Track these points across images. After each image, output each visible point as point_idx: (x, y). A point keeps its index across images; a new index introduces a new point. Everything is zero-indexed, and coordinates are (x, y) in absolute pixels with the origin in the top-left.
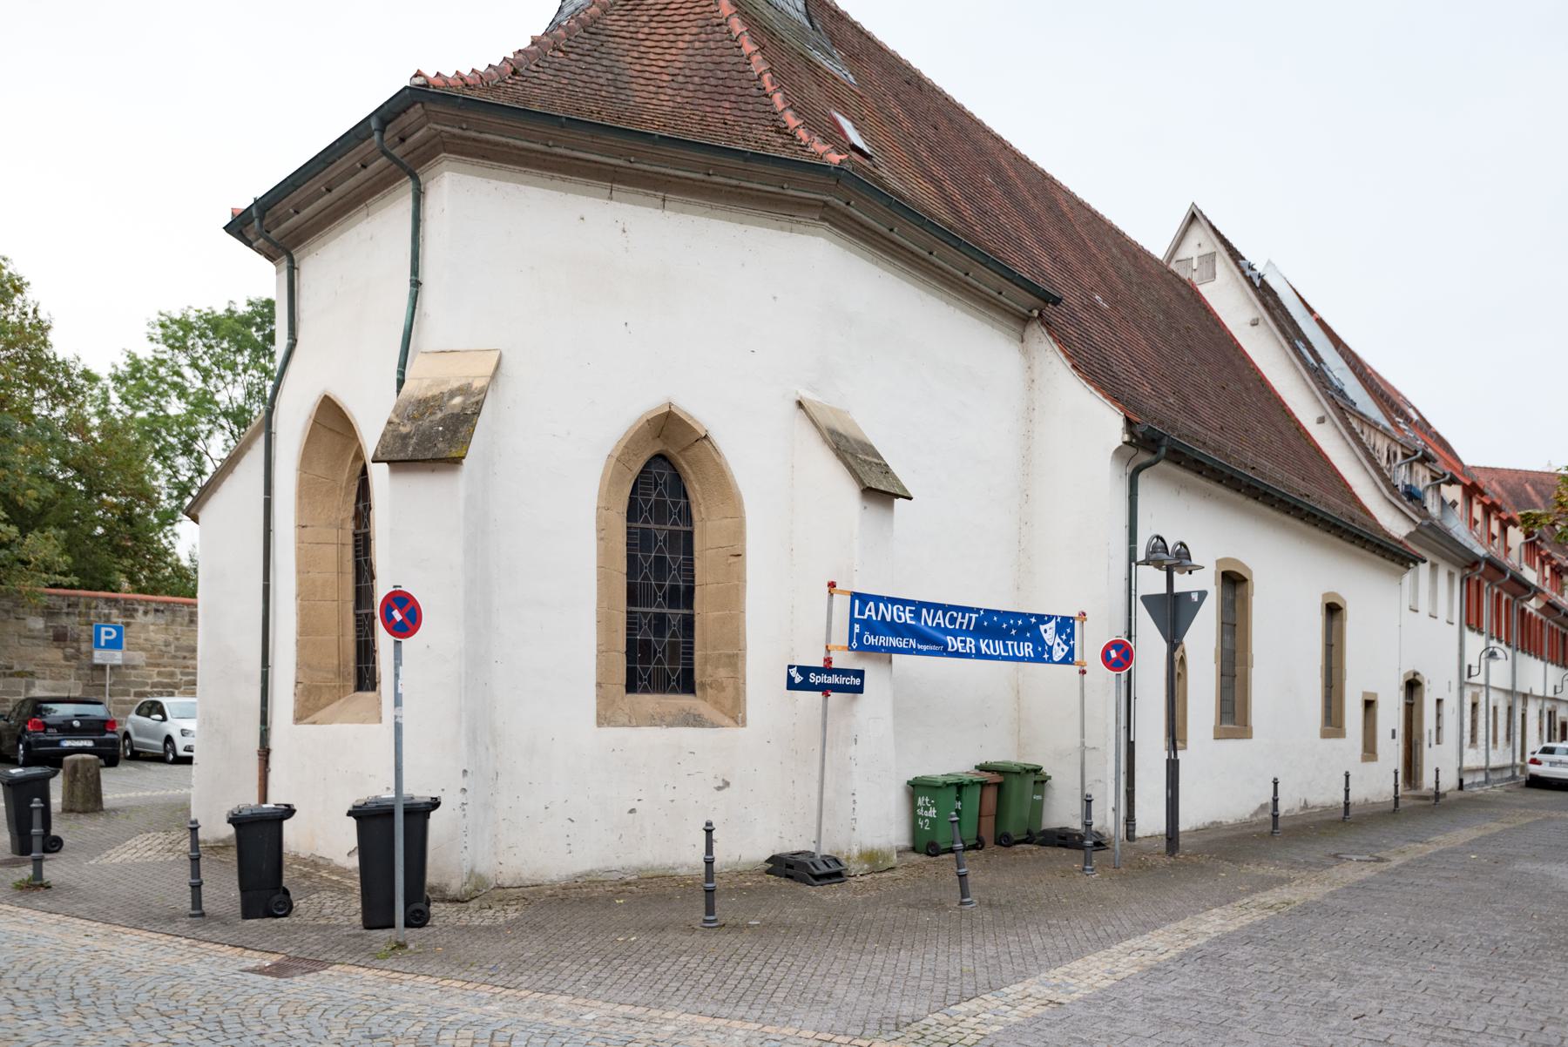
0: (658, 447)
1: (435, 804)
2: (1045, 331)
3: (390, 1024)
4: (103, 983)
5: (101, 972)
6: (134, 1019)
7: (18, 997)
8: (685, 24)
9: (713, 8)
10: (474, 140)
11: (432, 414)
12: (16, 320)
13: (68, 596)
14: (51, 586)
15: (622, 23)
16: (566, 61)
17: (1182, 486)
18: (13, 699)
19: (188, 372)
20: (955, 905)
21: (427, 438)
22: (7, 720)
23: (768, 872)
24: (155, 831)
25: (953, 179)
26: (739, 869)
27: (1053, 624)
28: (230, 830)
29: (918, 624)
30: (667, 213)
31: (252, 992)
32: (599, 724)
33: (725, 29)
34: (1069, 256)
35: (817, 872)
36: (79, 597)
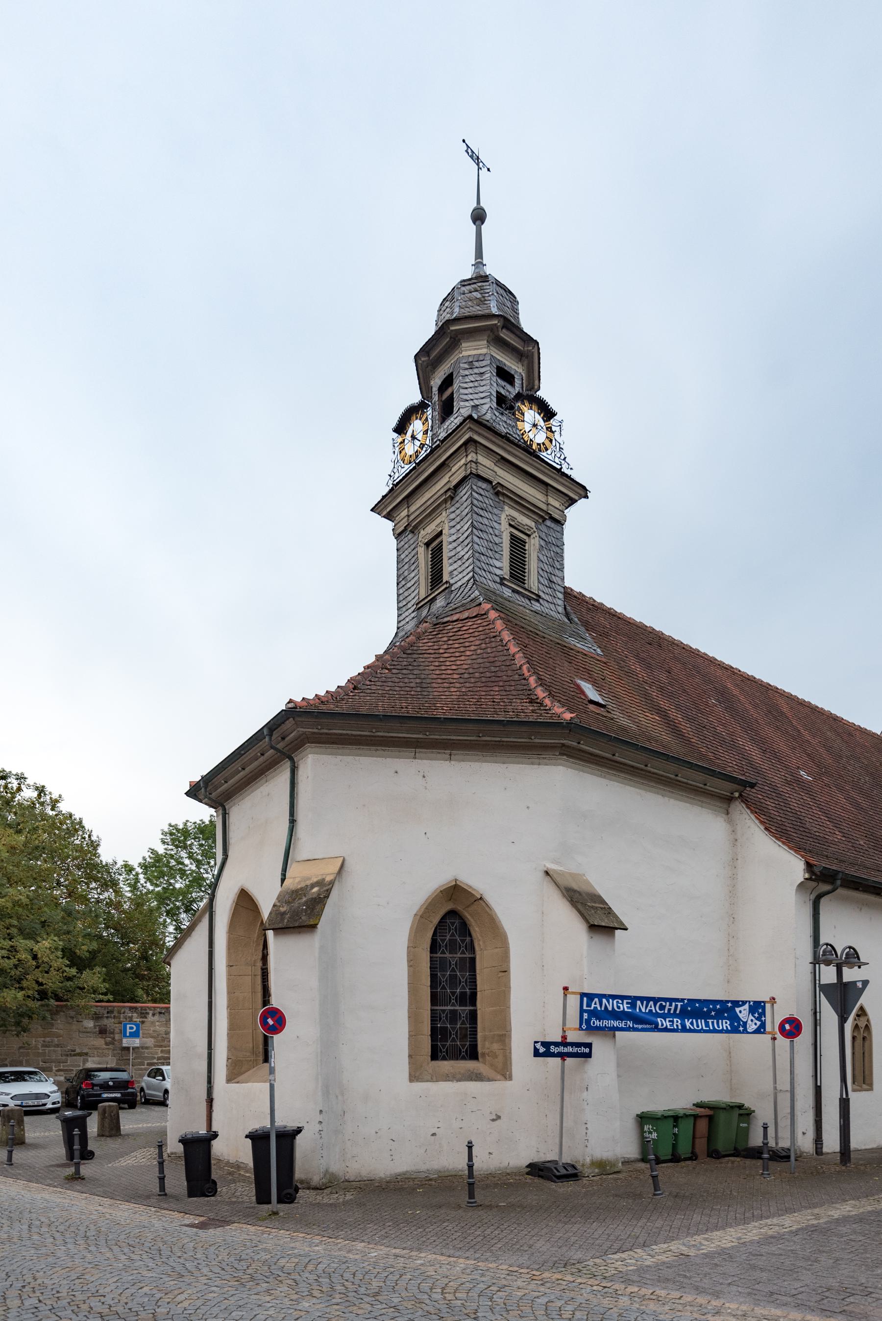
0: (449, 906)
1: (299, 1130)
2: (744, 806)
3: (253, 1254)
4: (103, 1229)
5: (103, 1224)
6: (115, 1248)
7: (57, 1235)
8: (472, 639)
9: (491, 626)
10: (326, 734)
11: (300, 899)
12: (79, 843)
13: (108, 1007)
14: (97, 1002)
15: (430, 644)
16: (390, 675)
17: (862, 905)
18: (76, 1069)
19: (187, 861)
20: (650, 1196)
21: (296, 914)
22: (72, 1082)
23: (528, 1174)
24: (149, 1147)
25: (678, 707)
26: (508, 1171)
27: (747, 1006)
28: (181, 1146)
29: (634, 1011)
30: (453, 762)
31: (182, 1236)
32: (411, 1081)
33: (498, 639)
34: (782, 746)
35: (558, 1174)
36: (114, 1007)
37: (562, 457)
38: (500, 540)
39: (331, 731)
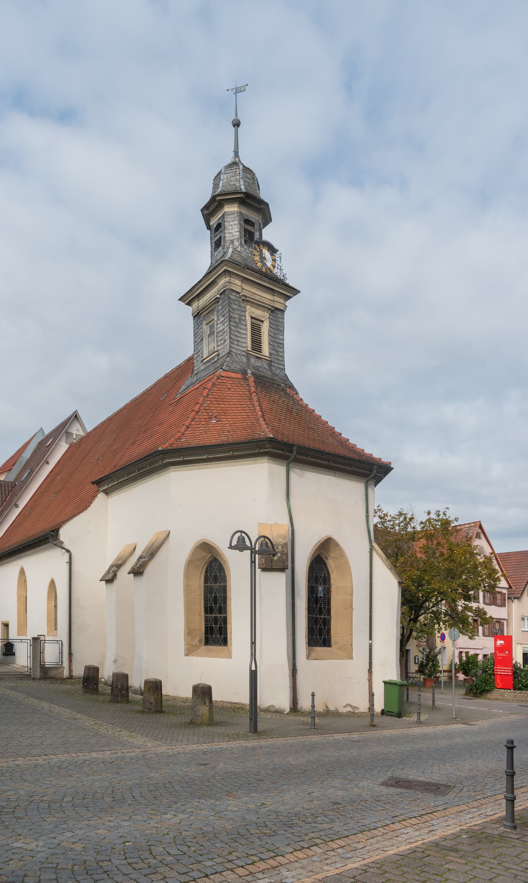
37: (282, 275)
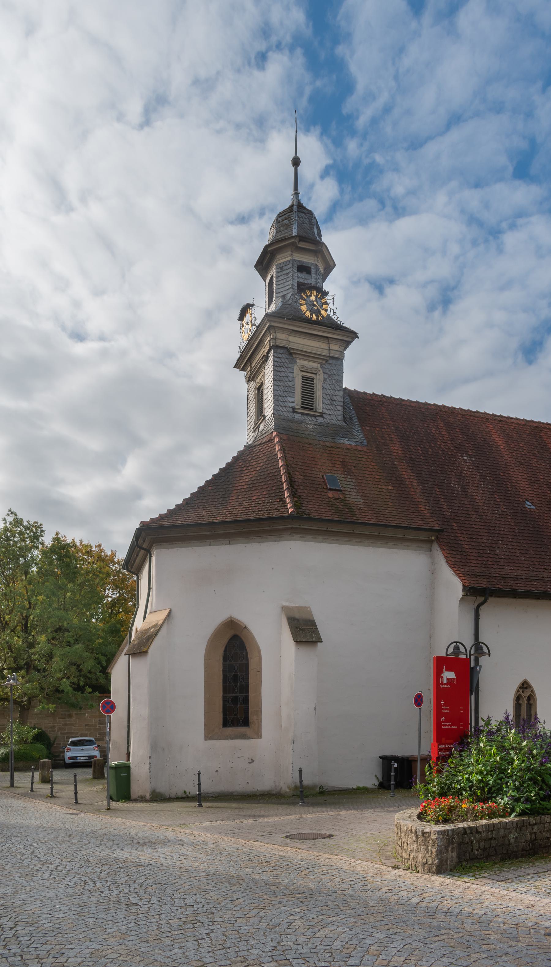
32: (205, 740)
38: (293, 383)
39: (164, 536)
